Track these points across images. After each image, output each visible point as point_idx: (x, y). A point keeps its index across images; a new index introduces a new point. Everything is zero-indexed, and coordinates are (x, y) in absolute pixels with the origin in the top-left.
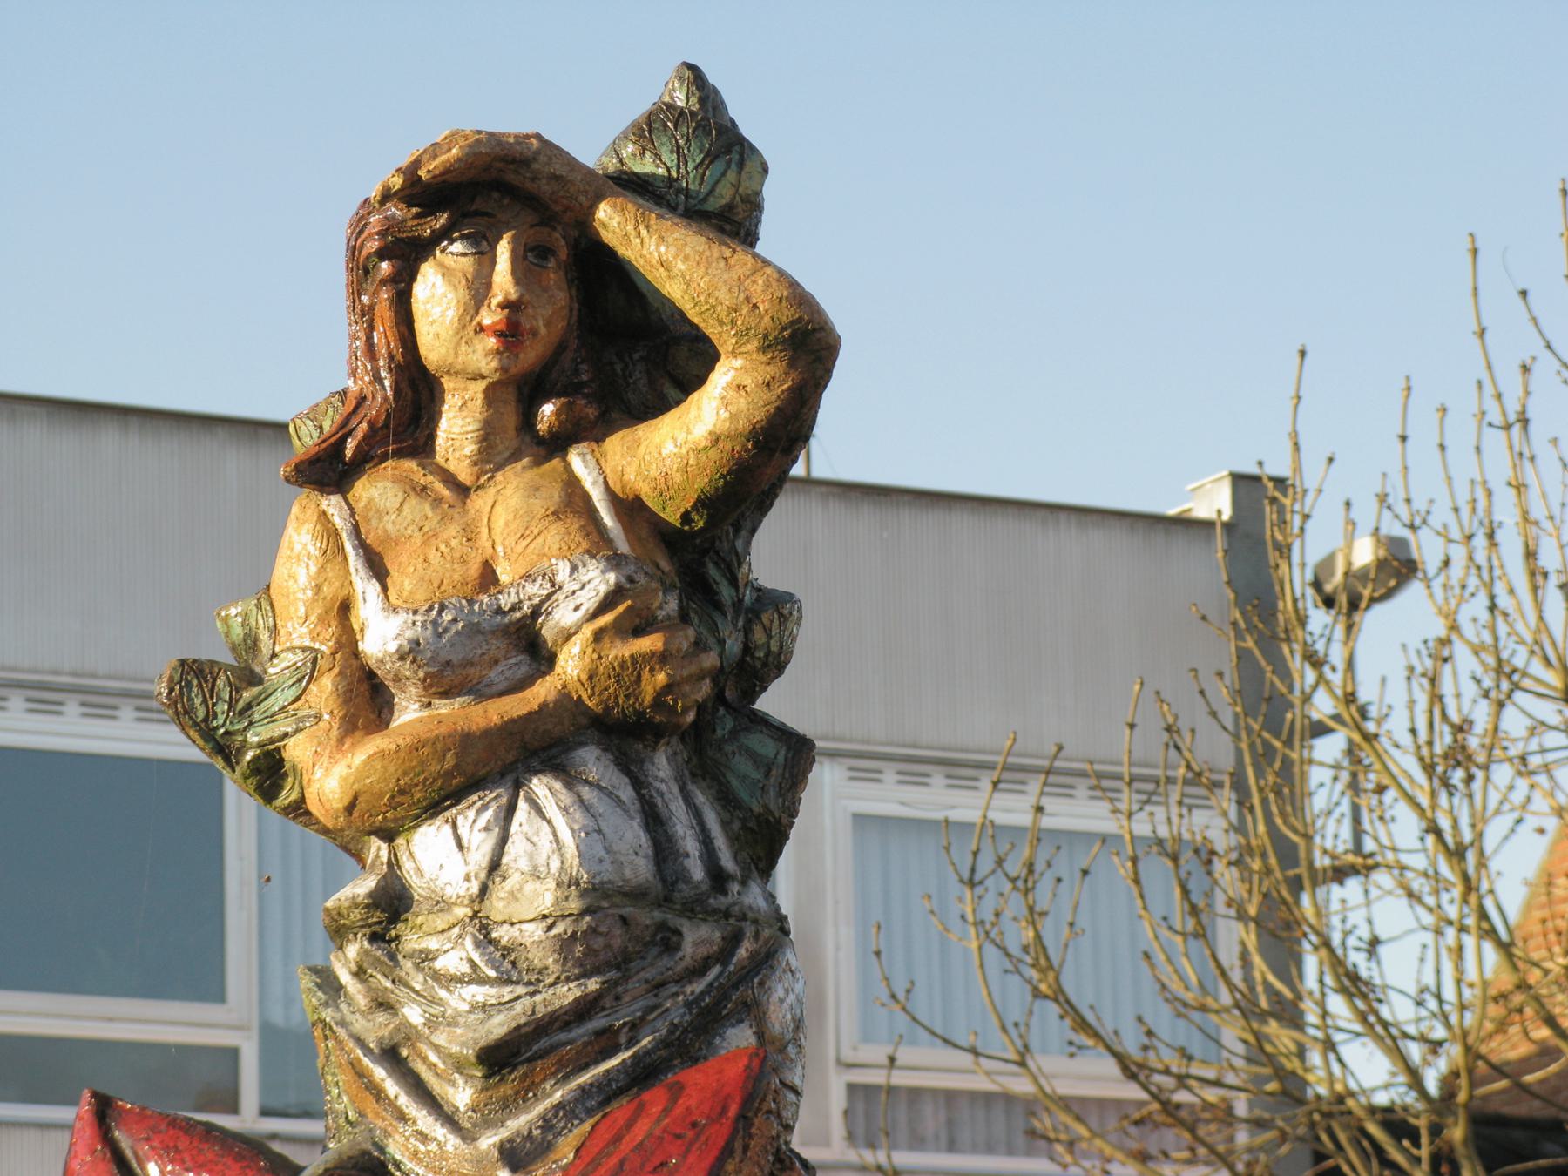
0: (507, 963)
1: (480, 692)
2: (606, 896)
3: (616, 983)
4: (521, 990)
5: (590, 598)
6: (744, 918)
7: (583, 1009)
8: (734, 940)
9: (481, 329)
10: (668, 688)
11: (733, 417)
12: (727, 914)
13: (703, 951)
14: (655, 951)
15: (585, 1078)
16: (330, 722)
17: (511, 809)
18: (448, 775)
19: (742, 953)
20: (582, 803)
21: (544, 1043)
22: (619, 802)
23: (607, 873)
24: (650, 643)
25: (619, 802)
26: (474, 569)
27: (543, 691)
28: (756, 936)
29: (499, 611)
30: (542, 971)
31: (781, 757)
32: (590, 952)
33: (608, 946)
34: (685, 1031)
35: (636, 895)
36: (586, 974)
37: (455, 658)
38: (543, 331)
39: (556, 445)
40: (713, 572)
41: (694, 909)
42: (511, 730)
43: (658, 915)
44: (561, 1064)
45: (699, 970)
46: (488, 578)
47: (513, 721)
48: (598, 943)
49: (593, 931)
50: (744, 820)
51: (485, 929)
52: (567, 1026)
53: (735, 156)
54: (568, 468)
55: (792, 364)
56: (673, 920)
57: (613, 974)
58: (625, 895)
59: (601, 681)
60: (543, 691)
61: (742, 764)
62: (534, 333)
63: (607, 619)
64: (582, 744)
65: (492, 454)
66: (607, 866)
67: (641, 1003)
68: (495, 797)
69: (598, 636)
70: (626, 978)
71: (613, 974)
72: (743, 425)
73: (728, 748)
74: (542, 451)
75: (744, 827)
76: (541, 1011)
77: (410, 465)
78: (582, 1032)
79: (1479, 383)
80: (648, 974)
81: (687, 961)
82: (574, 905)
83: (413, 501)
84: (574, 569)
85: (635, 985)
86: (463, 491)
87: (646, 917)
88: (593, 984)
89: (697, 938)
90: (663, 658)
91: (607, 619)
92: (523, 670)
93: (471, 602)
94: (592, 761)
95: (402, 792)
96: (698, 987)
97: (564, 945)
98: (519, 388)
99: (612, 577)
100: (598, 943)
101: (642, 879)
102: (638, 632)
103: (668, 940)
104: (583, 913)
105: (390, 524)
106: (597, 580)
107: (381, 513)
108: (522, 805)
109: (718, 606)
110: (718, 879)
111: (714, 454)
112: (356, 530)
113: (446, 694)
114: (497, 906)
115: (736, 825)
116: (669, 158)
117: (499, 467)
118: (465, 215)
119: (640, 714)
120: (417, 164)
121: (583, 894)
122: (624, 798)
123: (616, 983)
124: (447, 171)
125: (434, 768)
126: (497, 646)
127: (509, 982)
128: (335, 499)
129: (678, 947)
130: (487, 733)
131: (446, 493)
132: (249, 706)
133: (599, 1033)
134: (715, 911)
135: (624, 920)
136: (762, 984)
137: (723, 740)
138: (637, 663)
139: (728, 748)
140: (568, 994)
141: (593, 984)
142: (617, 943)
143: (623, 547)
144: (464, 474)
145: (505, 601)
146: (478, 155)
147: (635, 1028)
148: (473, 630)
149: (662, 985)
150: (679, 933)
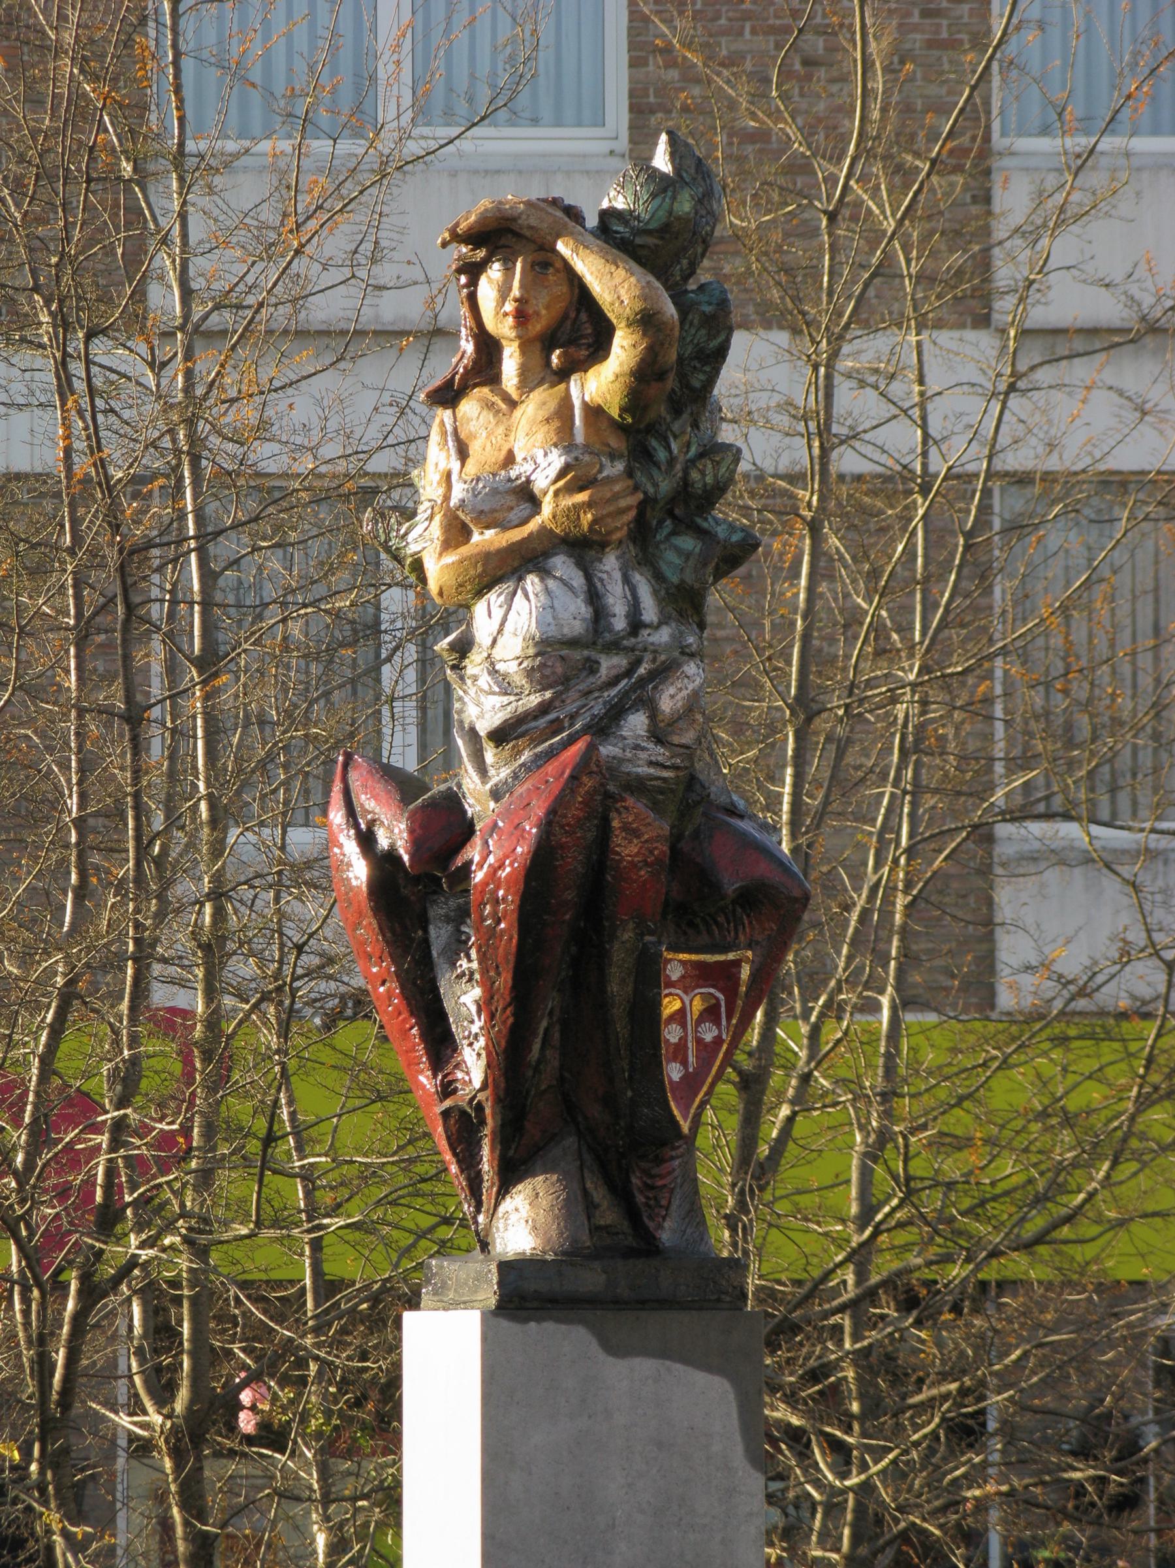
0: (505, 686)
1: (504, 526)
2: (550, 645)
3: (562, 693)
4: (512, 698)
5: (553, 472)
6: (645, 650)
7: (544, 709)
8: (638, 662)
9: (506, 314)
10: (595, 521)
11: (621, 364)
12: (633, 650)
13: (614, 672)
14: (585, 673)
15: (539, 749)
16: (437, 544)
17: (514, 593)
18: (480, 576)
19: (642, 670)
20: (547, 591)
21: (524, 728)
22: (571, 588)
23: (553, 632)
24: (582, 497)
25: (571, 588)
26: (504, 453)
27: (533, 525)
28: (654, 660)
29: (510, 480)
30: (522, 687)
31: (697, 550)
32: (543, 676)
33: (554, 673)
34: (602, 718)
35: (573, 643)
36: (544, 689)
37: (486, 508)
38: (544, 312)
39: (563, 375)
40: (654, 443)
41: (614, 647)
42: (512, 549)
43: (586, 653)
44: (532, 740)
45: (613, 682)
46: (510, 459)
47: (513, 544)
48: (547, 672)
49: (543, 666)
50: (667, 590)
51: (493, 664)
52: (535, 718)
53: (669, 194)
54: (568, 389)
55: (644, 335)
56: (594, 655)
57: (560, 688)
58: (563, 643)
59: (561, 519)
60: (533, 525)
61: (671, 556)
62: (537, 314)
63: (561, 483)
64: (556, 554)
65: (527, 382)
66: (553, 627)
67: (578, 703)
68: (507, 587)
69: (556, 494)
70: (567, 690)
71: (560, 688)
72: (626, 368)
73: (662, 547)
74: (555, 378)
75: (667, 593)
76: (520, 710)
77: (485, 391)
78: (542, 722)
79: (448, 475)
80: (581, 687)
81: (604, 678)
82: (531, 651)
83: (485, 412)
84: (546, 454)
85: (573, 694)
86: (513, 404)
87: (578, 655)
88: (548, 694)
89: (609, 664)
90: (589, 505)
91: (561, 483)
92: (526, 513)
93: (494, 475)
94: (562, 565)
95: (461, 586)
96: (613, 692)
97: (529, 673)
98: (543, 342)
99: (563, 459)
100: (547, 672)
101: (576, 633)
102: (581, 489)
103: (592, 667)
104: (536, 655)
105: (473, 426)
106: (557, 460)
107: (469, 420)
108: (519, 592)
109: (657, 465)
110: (636, 625)
111: (617, 385)
112: (455, 430)
113: (488, 527)
114: (497, 653)
115: (663, 593)
116: (631, 199)
117: (532, 390)
118: (497, 248)
119: (584, 536)
120: (457, 225)
121: (536, 644)
122: (575, 584)
123: (562, 693)
124: (470, 229)
125: (472, 572)
126: (510, 500)
127: (506, 694)
128: (449, 412)
129: (597, 671)
130: (499, 552)
131: (503, 406)
132: (406, 534)
133: (552, 722)
134: (625, 648)
135: (562, 658)
136: (655, 688)
137: (661, 542)
138: (577, 508)
139: (662, 547)
140: (534, 700)
141: (548, 694)
142: (559, 670)
143: (580, 437)
144: (515, 395)
145: (513, 474)
146: (486, 218)
147: (573, 717)
148: (495, 492)
149: (590, 692)
150: (598, 663)
